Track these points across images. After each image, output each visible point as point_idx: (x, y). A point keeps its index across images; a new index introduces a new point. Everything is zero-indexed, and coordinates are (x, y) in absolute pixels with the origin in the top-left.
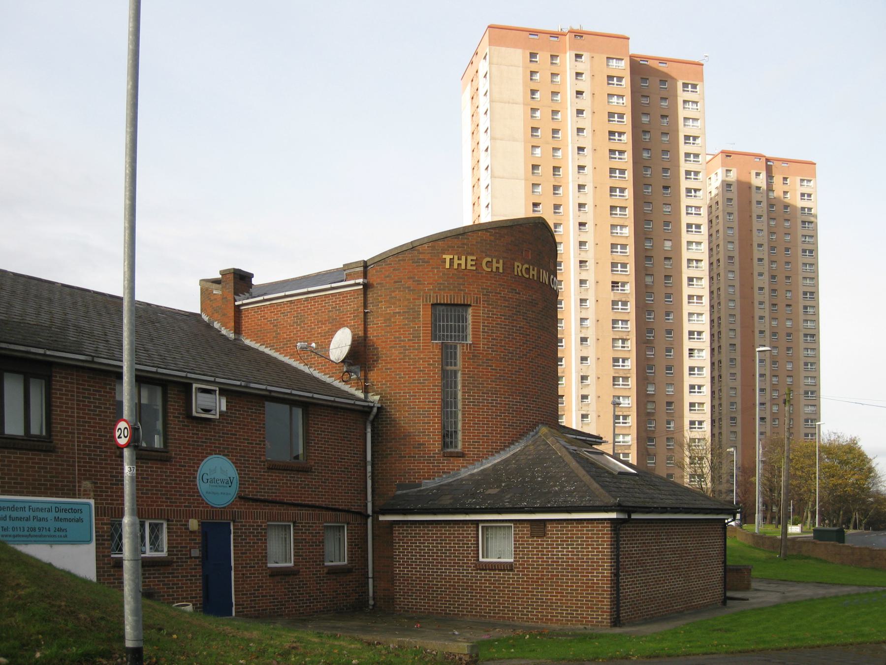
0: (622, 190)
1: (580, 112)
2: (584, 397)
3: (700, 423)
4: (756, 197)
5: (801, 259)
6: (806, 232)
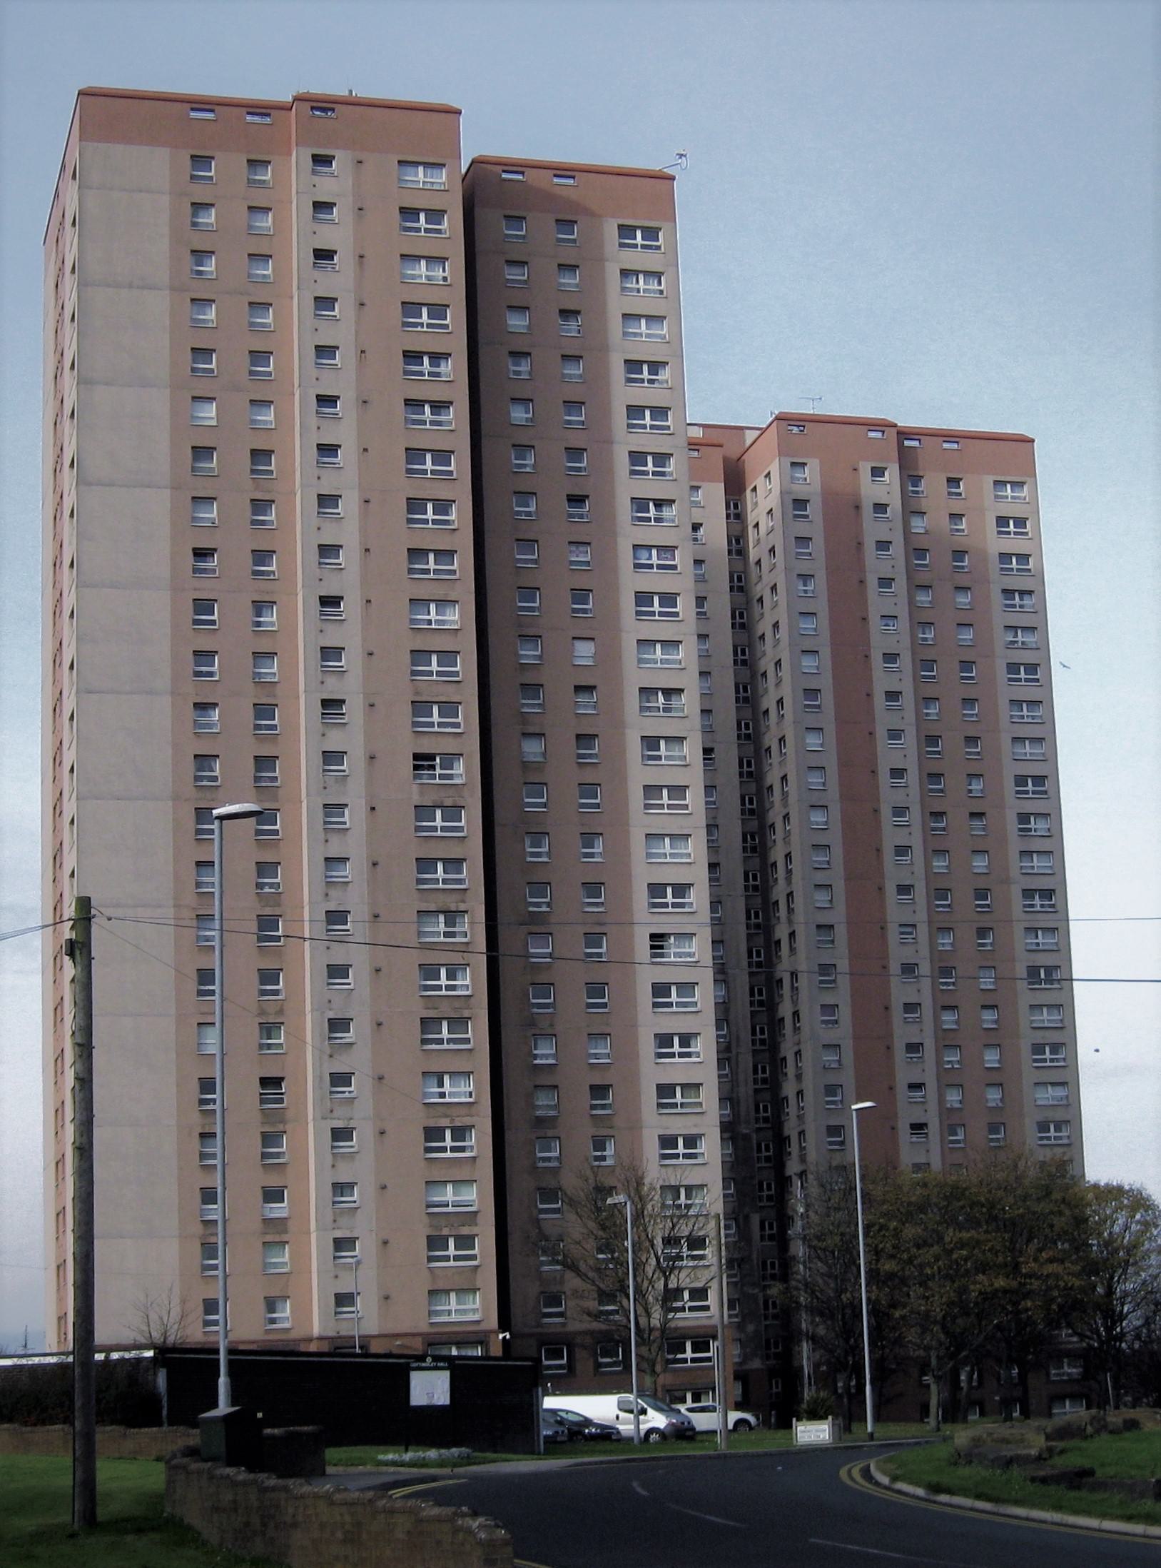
0: (442, 506)
1: (325, 303)
2: (340, 1079)
3: (691, 1141)
4: (873, 530)
5: (1005, 691)
6: (1014, 620)
